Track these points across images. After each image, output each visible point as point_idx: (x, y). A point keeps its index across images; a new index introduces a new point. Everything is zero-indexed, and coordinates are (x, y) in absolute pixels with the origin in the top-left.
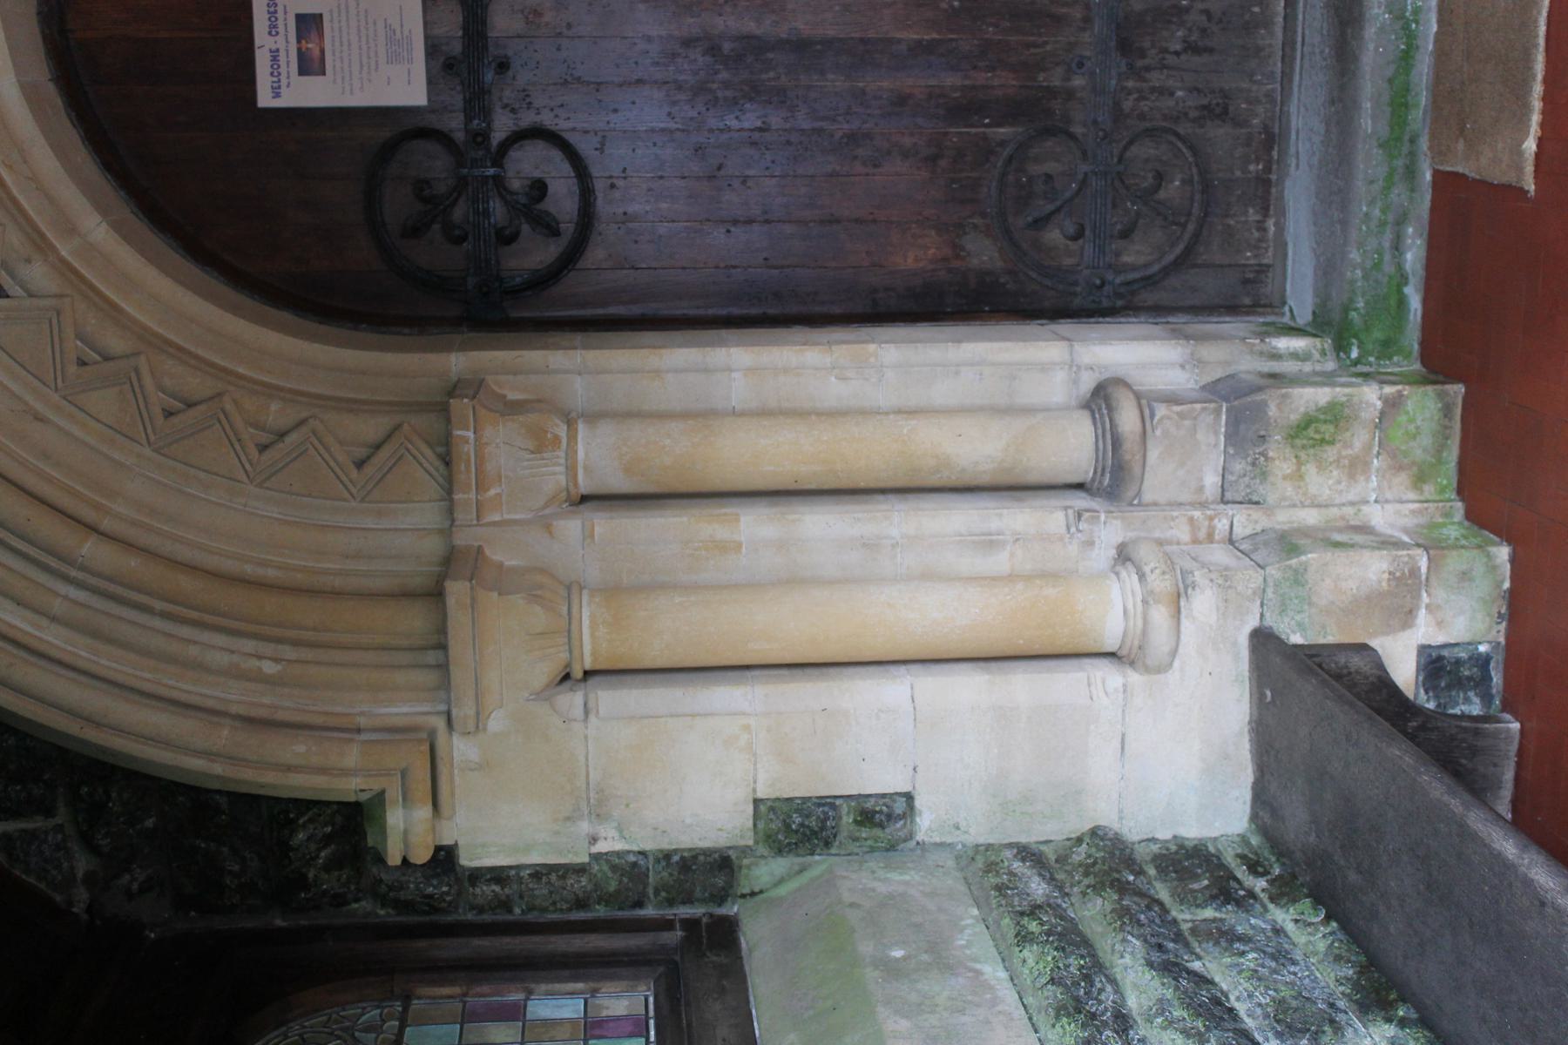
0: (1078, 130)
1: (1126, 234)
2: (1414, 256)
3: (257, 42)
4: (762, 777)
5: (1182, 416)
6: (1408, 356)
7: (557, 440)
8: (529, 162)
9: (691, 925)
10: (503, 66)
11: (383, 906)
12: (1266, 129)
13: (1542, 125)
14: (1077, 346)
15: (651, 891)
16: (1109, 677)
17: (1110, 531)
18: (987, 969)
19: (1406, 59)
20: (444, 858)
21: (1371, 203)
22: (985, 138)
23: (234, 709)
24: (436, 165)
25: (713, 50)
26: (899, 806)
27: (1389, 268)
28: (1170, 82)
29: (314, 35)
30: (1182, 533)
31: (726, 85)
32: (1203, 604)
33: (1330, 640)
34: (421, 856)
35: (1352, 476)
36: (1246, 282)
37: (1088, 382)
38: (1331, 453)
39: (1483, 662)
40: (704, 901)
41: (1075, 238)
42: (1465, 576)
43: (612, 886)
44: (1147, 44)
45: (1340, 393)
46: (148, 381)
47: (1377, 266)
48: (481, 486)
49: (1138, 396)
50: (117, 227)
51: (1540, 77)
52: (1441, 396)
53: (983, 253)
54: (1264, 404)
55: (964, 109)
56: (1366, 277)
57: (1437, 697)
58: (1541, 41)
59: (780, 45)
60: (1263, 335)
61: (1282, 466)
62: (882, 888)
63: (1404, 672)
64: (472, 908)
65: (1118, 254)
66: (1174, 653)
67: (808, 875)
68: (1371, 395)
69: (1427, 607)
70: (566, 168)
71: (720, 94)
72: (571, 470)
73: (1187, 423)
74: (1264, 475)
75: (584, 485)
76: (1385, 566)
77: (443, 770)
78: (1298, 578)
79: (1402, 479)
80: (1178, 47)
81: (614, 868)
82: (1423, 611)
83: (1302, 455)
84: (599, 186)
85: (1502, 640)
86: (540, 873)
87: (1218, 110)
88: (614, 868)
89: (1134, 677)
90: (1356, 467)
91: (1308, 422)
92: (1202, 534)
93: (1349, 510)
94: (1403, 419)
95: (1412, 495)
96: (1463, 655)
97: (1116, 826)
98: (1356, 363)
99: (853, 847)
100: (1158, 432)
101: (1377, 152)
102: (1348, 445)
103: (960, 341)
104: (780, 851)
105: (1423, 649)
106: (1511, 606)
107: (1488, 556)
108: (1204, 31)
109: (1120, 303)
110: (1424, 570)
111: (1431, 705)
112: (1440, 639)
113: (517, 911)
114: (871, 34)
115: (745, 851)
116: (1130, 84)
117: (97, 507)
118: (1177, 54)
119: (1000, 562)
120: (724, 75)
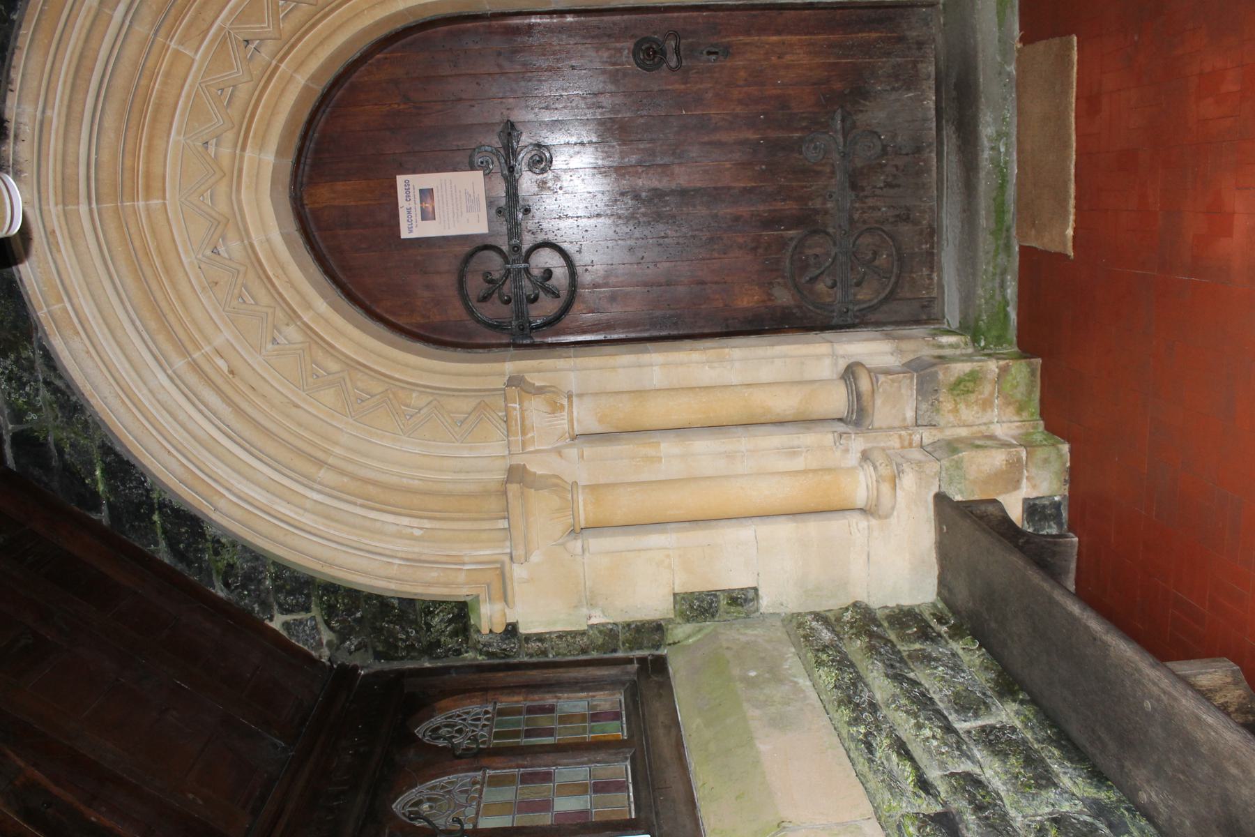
0: (831, 230)
1: (858, 284)
2: (1011, 291)
3: (400, 205)
4: (677, 582)
5: (893, 381)
6: (1010, 344)
7: (562, 406)
8: (546, 259)
9: (642, 660)
10: (527, 211)
11: (481, 654)
12: (930, 226)
13: (1076, 221)
14: (837, 346)
15: (620, 643)
16: (859, 523)
17: (857, 444)
18: (801, 681)
19: (1002, 187)
20: (511, 630)
21: (988, 264)
22: (782, 237)
23: (399, 555)
24: (494, 263)
25: (637, 197)
26: (751, 594)
27: (998, 298)
28: (878, 203)
29: (429, 200)
30: (895, 442)
31: (644, 215)
32: (908, 481)
33: (976, 497)
34: (499, 629)
35: (984, 410)
36: (923, 307)
37: (842, 364)
38: (972, 397)
39: (1057, 506)
40: (648, 648)
41: (832, 287)
42: (1046, 461)
43: (600, 641)
44: (865, 184)
45: (976, 366)
46: (348, 380)
47: (992, 297)
48: (524, 433)
49: (869, 371)
50: (332, 305)
51: (1073, 195)
52: (1029, 365)
53: (783, 297)
54: (936, 372)
55: (770, 222)
56: (986, 303)
57: (1033, 525)
58: (1073, 177)
59: (672, 192)
60: (933, 336)
61: (948, 406)
62: (743, 639)
63: (1016, 513)
64: (527, 655)
65: (855, 295)
66: (893, 508)
67: (706, 631)
68: (993, 366)
69: (1027, 478)
70: (561, 262)
71: (641, 220)
72: (571, 421)
73: (896, 384)
74: (938, 411)
75: (578, 429)
76: (1004, 457)
77: (508, 582)
78: (958, 465)
79: (1010, 412)
80: (882, 185)
81: (600, 632)
82: (1025, 480)
83: (958, 399)
84: (580, 270)
85: (1067, 494)
86: (562, 636)
87: (905, 217)
88: (600, 632)
89: (874, 522)
90: (986, 404)
91: (959, 382)
92: (906, 443)
93: (983, 428)
94: (1009, 378)
95: (1016, 418)
96: (1047, 503)
97: (866, 601)
98: (983, 348)
99: (727, 617)
100: (881, 390)
101: (990, 238)
102: (981, 393)
103: (773, 345)
104: (688, 620)
105: (1026, 500)
106: (1071, 475)
107: (1058, 449)
108: (895, 176)
109: (857, 321)
110: (1024, 458)
111: (1030, 530)
112: (1034, 495)
113: (551, 656)
114: (719, 185)
115: (669, 621)
116: (857, 205)
117: (325, 451)
118: (881, 188)
119: (799, 464)
120: (643, 210)
